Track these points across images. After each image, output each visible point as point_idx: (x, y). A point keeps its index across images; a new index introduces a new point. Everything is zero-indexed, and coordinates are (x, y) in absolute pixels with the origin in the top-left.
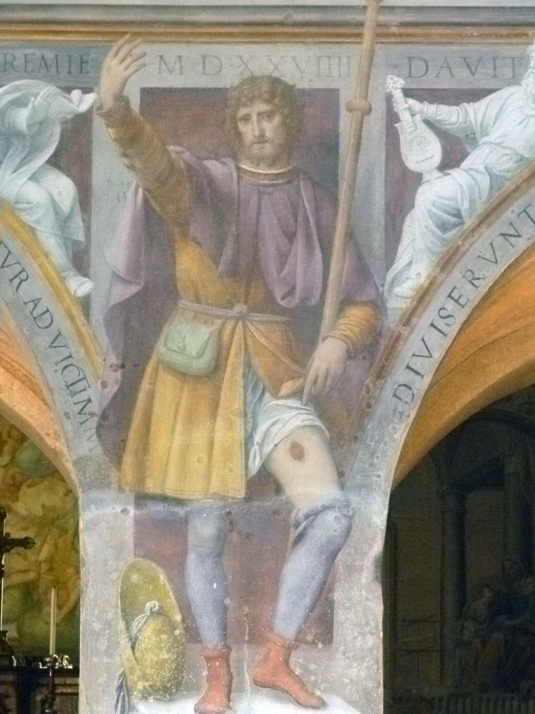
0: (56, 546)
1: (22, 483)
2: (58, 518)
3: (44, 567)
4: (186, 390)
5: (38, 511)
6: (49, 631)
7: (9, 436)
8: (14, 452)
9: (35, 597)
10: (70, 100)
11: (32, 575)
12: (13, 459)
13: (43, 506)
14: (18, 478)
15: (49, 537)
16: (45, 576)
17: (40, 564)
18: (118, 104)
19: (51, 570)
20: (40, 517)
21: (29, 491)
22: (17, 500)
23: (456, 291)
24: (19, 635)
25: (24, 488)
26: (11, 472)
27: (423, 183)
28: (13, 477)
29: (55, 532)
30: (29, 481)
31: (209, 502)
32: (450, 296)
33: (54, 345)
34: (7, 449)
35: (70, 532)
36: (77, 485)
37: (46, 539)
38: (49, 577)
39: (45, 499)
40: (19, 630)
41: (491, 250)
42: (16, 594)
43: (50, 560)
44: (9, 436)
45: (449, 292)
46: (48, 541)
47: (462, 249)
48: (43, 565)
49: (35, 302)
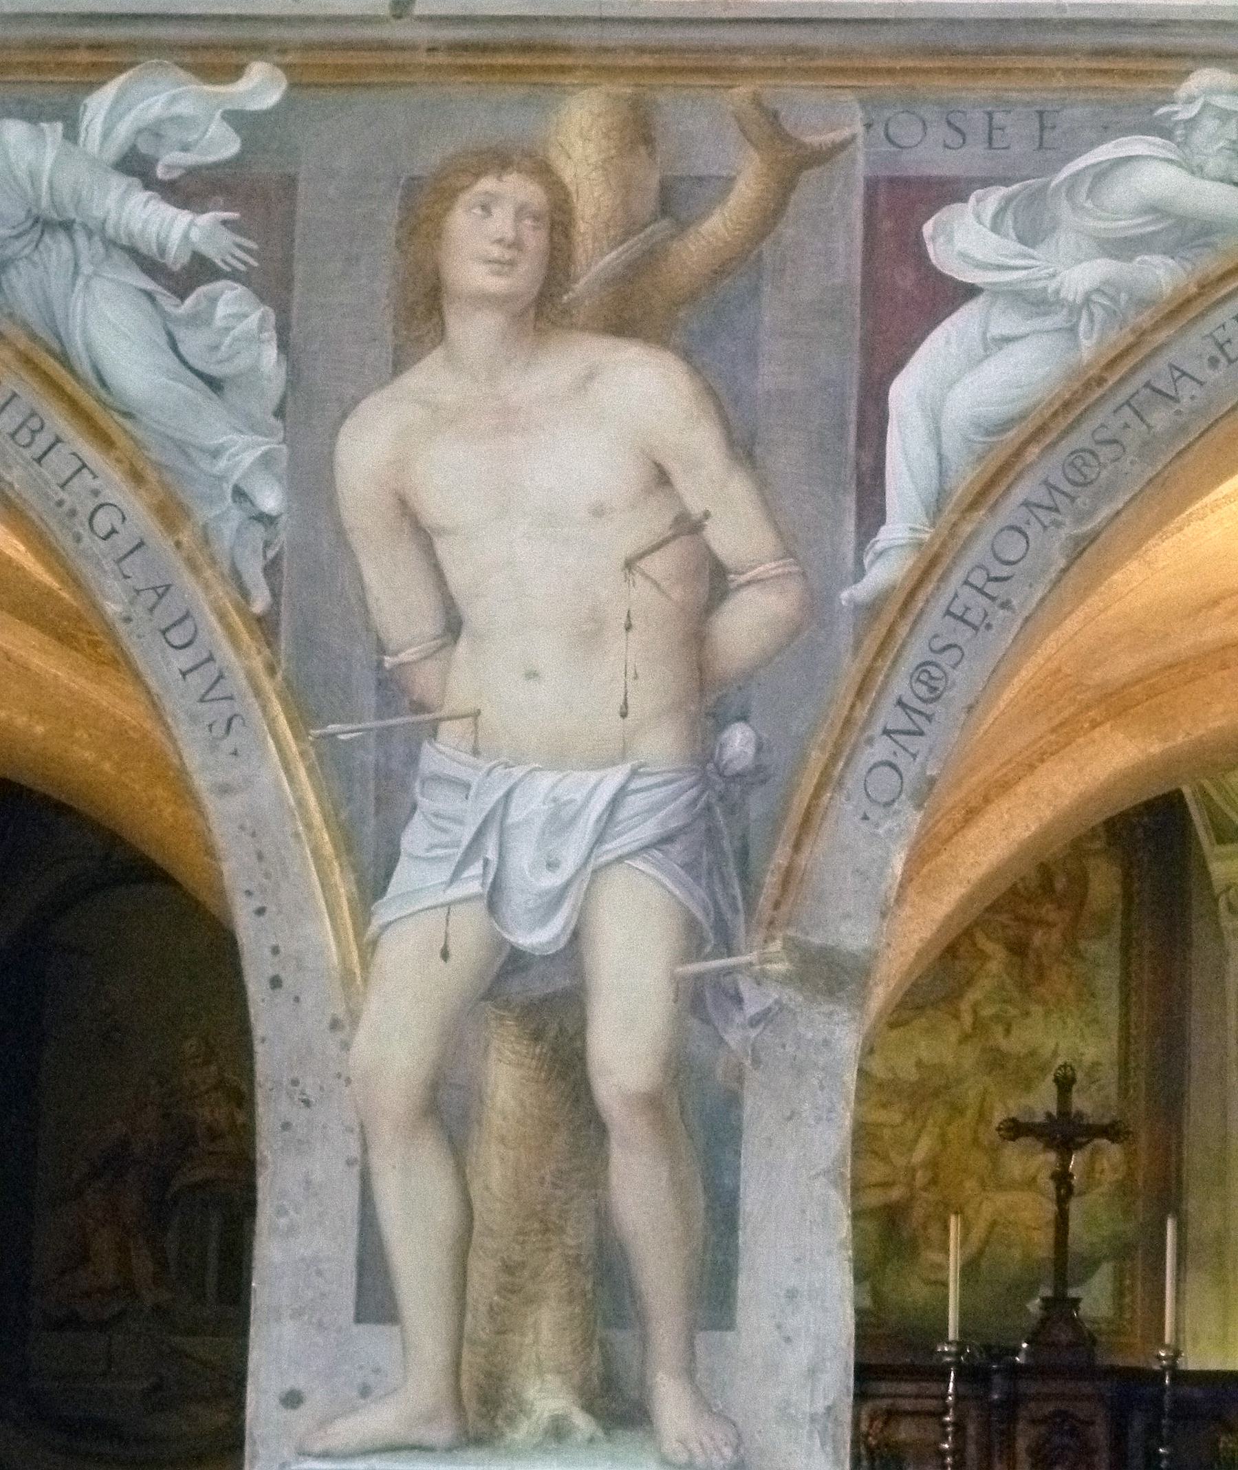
0: (943, 1139)
2: (947, 1087)
3: (921, 1177)
5: (909, 1073)
6: (946, 1297)
11: (896, 1194)
13: (919, 1064)
15: (931, 1121)
16: (924, 1194)
17: (914, 1170)
19: (934, 1181)
20: (912, 1084)
23: (956, 603)
24: (875, 1302)
27: (185, 168)
29: (941, 1113)
32: (948, 613)
33: (212, 695)
35: (970, 1113)
37: (924, 1126)
38: (932, 1196)
41: (192, 361)
43: (933, 1164)
46: (929, 1128)
47: (23, 343)
48: (919, 1174)
49: (160, 591)
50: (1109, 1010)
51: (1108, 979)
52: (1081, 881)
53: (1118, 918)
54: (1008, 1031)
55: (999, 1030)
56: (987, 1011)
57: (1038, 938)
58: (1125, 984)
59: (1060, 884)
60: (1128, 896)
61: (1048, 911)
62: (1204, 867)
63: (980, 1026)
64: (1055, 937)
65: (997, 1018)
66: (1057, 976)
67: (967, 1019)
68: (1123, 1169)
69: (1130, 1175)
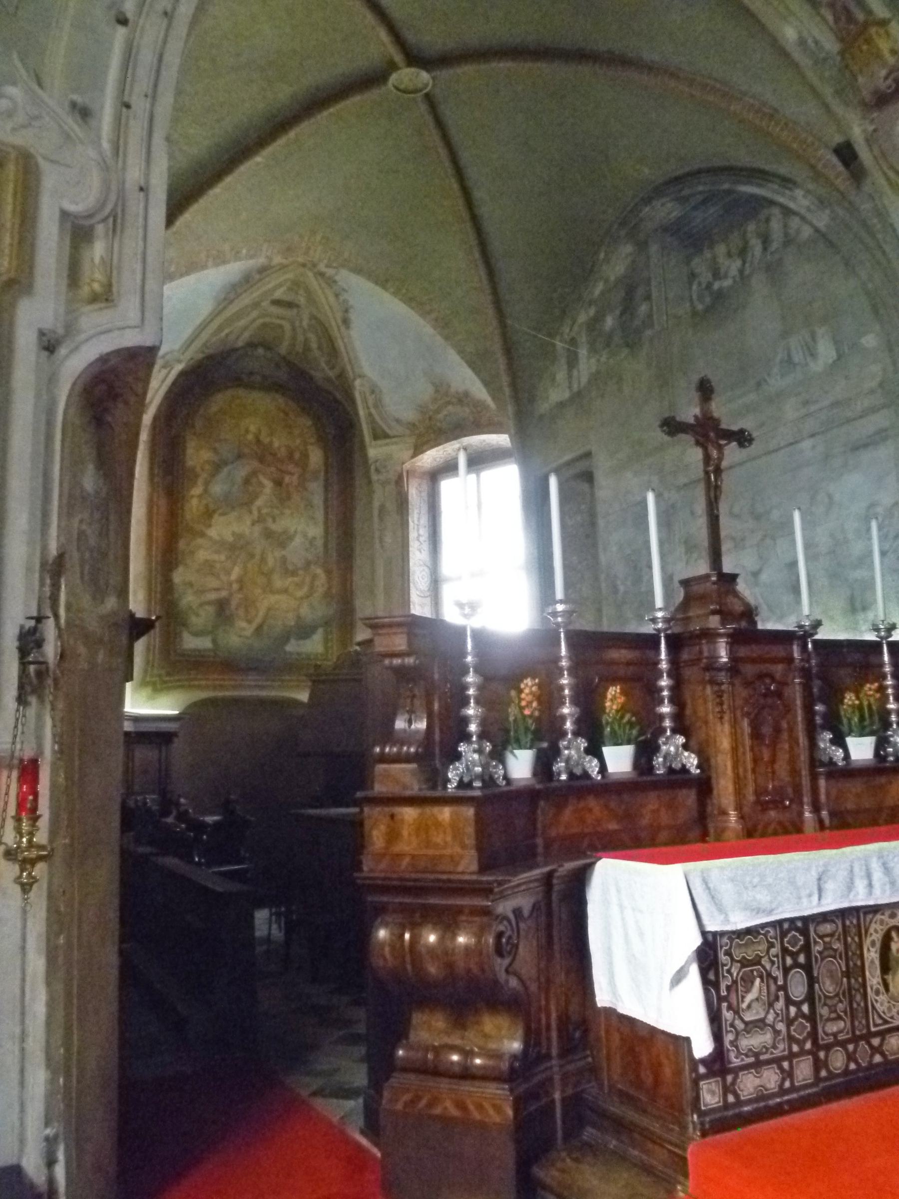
1: (214, 511)
3: (235, 586)
4: (541, 888)
7: (203, 470)
8: (207, 484)
9: (228, 613)
10: (371, 442)
11: (224, 594)
12: (206, 491)
13: (234, 534)
14: (212, 506)
18: (703, 736)
21: (222, 519)
22: (210, 526)
25: (216, 516)
26: (204, 502)
28: (207, 506)
30: (220, 511)
31: (613, 1106)
34: (200, 481)
35: (258, 557)
36: (218, 337)
39: (236, 528)
40: (214, 641)
42: (211, 609)
43: (240, 581)
44: (203, 470)
45: (151, 197)
50: (320, 515)
51: (318, 500)
52: (305, 456)
53: (322, 474)
54: (274, 521)
55: (270, 520)
56: (264, 511)
57: (287, 479)
58: (326, 500)
59: (297, 456)
60: (326, 464)
61: (291, 467)
62: (363, 448)
63: (260, 520)
64: (295, 478)
65: (267, 514)
66: (296, 497)
67: (255, 513)
68: (326, 586)
69: (330, 588)
